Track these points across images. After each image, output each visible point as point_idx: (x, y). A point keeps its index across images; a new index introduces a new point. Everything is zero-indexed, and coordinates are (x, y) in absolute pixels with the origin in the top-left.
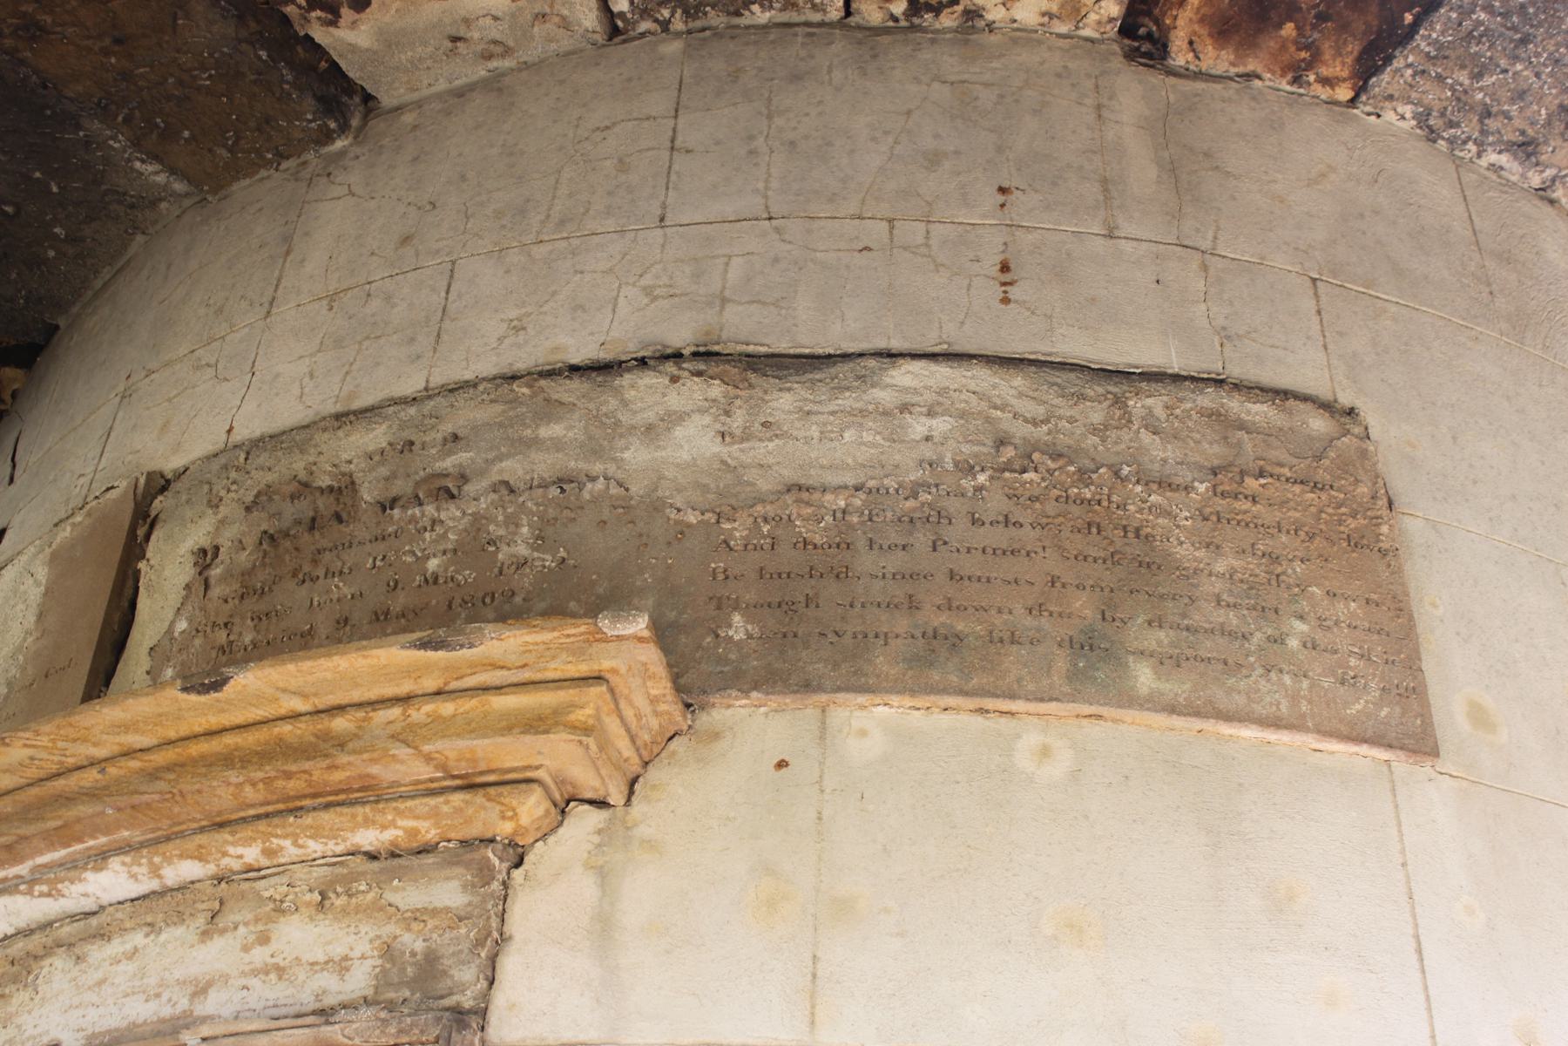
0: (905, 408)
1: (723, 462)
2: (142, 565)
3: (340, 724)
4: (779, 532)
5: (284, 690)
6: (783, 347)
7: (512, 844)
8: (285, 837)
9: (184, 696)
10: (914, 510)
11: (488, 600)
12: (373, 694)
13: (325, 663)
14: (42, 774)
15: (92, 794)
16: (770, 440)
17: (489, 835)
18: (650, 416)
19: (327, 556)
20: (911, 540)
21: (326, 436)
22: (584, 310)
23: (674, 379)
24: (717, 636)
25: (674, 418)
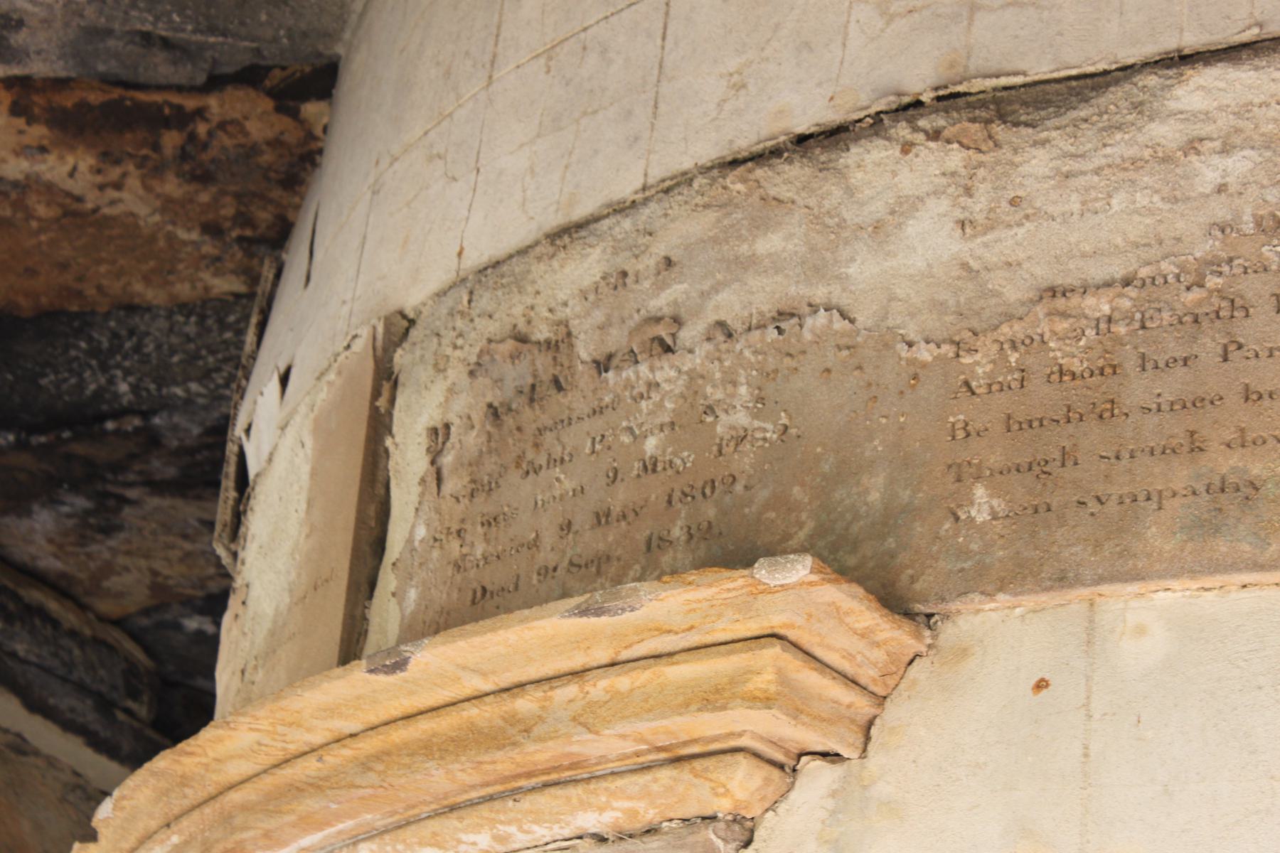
0: (1192, 146)
1: (965, 266)
2: (388, 442)
3: (524, 704)
4: (1030, 360)
5: (464, 668)
6: (1041, 69)
7: (737, 820)
8: (509, 823)
9: (373, 677)
10: (1199, 303)
11: (708, 491)
12: (548, 669)
13: (502, 635)
14: (272, 760)
15: (316, 786)
16: (1020, 225)
17: (709, 813)
18: (877, 209)
19: (549, 437)
20: (1196, 350)
21: (542, 267)
22: (811, 50)
23: (907, 148)
24: (957, 519)
25: (905, 207)
